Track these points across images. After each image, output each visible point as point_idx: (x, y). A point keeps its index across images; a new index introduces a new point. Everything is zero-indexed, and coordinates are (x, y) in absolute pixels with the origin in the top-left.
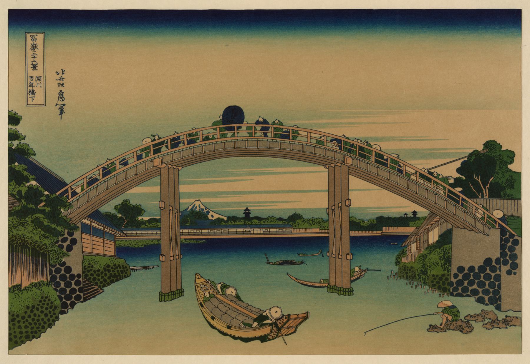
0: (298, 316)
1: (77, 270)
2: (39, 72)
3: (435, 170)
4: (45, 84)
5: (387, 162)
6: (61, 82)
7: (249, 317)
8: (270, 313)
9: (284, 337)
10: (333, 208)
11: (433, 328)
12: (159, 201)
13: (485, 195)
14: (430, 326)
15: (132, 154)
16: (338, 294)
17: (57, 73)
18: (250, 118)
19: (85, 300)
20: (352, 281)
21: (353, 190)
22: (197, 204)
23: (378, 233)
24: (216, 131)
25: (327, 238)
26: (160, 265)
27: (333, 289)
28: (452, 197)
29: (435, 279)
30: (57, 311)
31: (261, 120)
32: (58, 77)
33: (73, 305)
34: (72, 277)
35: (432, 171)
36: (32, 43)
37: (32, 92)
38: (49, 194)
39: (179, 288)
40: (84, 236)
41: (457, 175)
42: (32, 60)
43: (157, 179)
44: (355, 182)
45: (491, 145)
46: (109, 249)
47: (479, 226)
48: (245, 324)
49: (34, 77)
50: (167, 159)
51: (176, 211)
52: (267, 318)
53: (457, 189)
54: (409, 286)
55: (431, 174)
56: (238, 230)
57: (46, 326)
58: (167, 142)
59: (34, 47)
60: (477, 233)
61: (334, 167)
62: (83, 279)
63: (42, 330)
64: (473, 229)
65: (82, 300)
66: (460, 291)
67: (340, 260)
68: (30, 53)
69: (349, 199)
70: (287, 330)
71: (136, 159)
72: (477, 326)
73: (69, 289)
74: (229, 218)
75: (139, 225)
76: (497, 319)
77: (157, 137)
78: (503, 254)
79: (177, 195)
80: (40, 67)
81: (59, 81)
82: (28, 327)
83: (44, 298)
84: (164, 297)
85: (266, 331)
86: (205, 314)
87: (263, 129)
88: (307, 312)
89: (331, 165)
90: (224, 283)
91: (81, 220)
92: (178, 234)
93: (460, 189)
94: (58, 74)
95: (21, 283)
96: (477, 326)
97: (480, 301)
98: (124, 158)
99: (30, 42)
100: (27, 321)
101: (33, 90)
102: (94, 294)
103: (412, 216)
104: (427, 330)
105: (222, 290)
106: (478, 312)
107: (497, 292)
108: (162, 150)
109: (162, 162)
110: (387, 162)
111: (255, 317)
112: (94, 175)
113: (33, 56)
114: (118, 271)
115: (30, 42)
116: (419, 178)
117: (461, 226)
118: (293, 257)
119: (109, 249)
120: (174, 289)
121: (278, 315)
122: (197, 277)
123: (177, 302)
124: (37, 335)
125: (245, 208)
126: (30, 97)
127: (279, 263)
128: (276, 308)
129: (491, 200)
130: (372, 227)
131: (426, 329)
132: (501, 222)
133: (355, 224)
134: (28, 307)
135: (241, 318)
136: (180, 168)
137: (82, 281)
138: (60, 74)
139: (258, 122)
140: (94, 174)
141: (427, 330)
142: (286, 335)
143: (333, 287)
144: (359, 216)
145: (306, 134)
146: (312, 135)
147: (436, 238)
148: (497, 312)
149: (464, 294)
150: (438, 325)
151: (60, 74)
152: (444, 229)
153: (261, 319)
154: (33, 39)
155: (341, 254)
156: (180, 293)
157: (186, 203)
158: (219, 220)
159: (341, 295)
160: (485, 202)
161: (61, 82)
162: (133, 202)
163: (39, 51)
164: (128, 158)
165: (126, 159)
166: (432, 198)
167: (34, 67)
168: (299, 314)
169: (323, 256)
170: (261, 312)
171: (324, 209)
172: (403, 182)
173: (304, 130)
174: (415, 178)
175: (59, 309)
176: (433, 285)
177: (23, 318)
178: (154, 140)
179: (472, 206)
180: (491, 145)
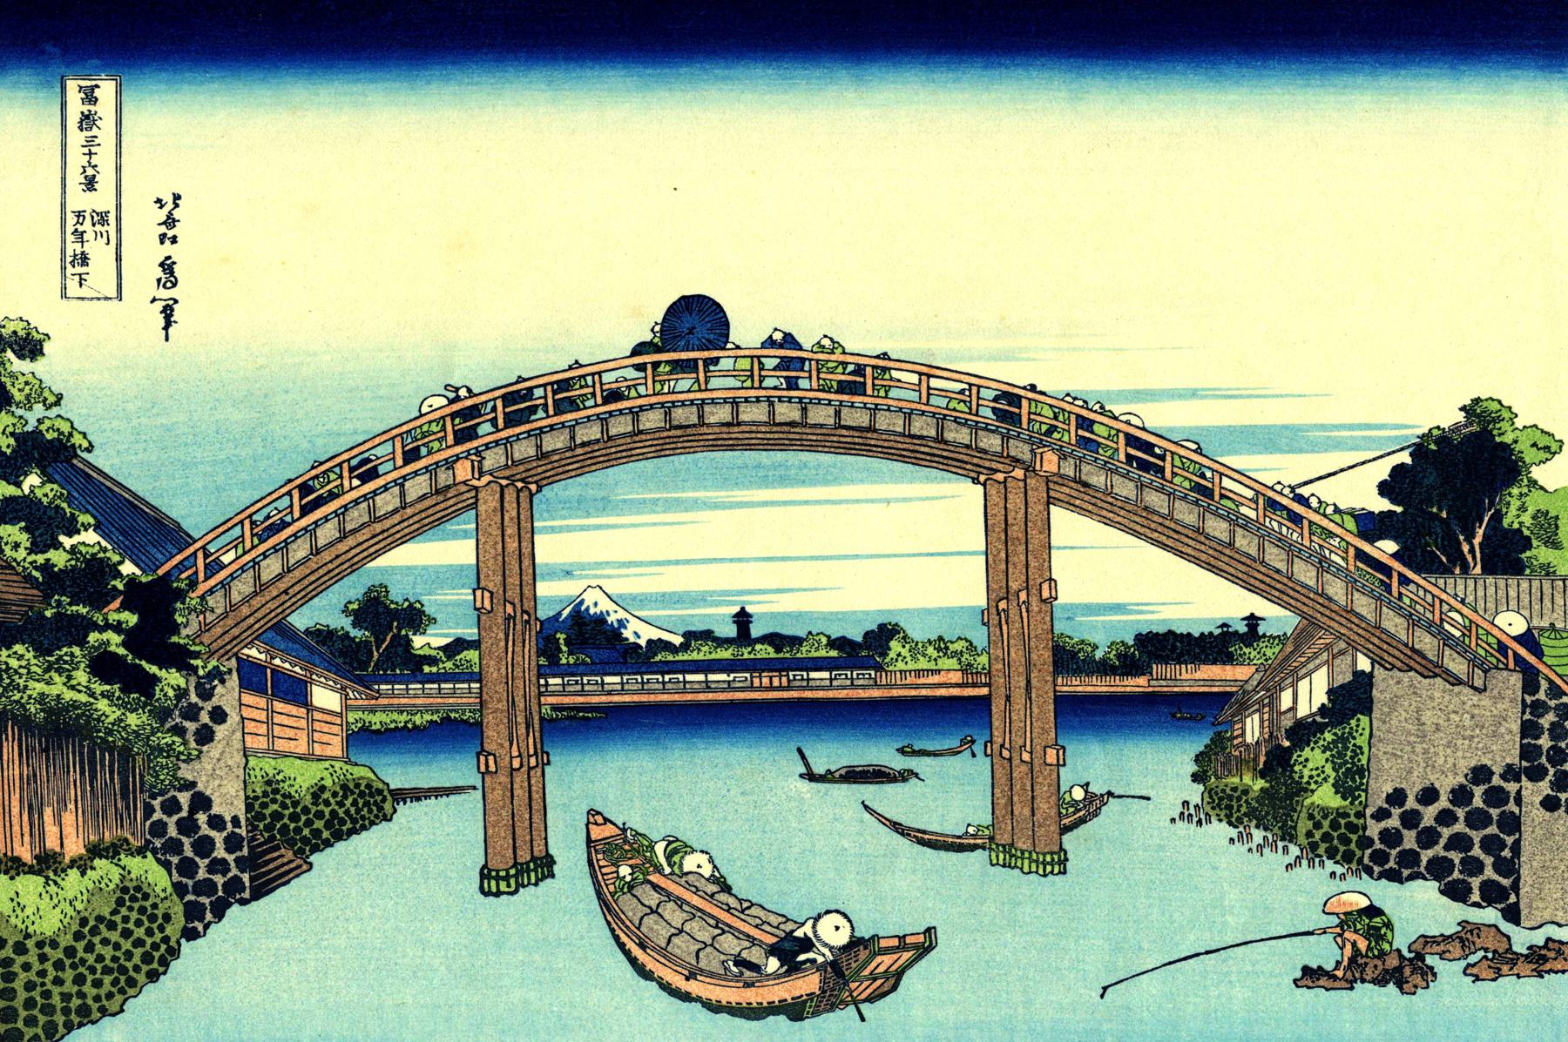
0: (902, 944)
1: (228, 800)
2: (102, 199)
4: (119, 230)
5: (1161, 463)
7: (753, 941)
8: (815, 932)
9: (863, 1007)
10: (1003, 605)
11: (1311, 976)
12: (474, 590)
13: (1472, 565)
14: (1306, 970)
15: (388, 448)
16: (1021, 869)
17: (159, 201)
18: (747, 330)
19: (258, 894)
20: (1066, 830)
21: (1059, 548)
22: (590, 598)
23: (1136, 684)
24: (643, 374)
25: (986, 701)
26: (479, 785)
29: (1318, 826)
30: (173, 930)
31: (778, 336)
32: (162, 215)
33: (219, 912)
34: (217, 822)
35: (1305, 491)
37: (84, 259)
38: (138, 572)
39: (539, 851)
40: (248, 698)
41: (1382, 505)
43: (467, 523)
44: (1067, 525)
45: (1472, 410)
46: (326, 738)
47: (1457, 665)
48: (740, 962)
50: (493, 459)
52: (806, 944)
53: (1382, 544)
54: (1239, 848)
55: (1302, 500)
56: (712, 677)
57: (141, 978)
58: (494, 409)
59: (87, 120)
60: (1425, 677)
62: (248, 832)
63: (131, 992)
64: (1437, 670)
65: (247, 895)
66: (1391, 864)
67: (1024, 768)
68: (76, 138)
69: (1051, 579)
70: (868, 983)
71: (400, 462)
72: (1449, 972)
73: (207, 861)
74: (689, 636)
75: (413, 666)
77: (463, 393)
78: (1528, 752)
79: (526, 567)
80: (106, 181)
81: (163, 229)
82: (94, 973)
83: (132, 893)
84: (493, 881)
85: (808, 984)
86: (618, 932)
87: (785, 363)
88: (928, 930)
89: (994, 477)
90: (677, 840)
91: (236, 650)
92: (534, 690)
93: (1390, 546)
94: (161, 207)
96: (1449, 972)
97: (1456, 892)
98: (366, 455)
99: (76, 106)
100: (83, 961)
101: (83, 253)
102: (282, 878)
103: (1242, 629)
104: (1295, 981)
105: (668, 858)
106: (1452, 929)
107: (1508, 867)
108: (482, 430)
109: (480, 469)
110: (1161, 463)
111: (771, 940)
112: (275, 512)
113: (86, 150)
115: (76, 106)
116: (1265, 516)
117: (1399, 664)
118: (882, 753)
119: (326, 738)
120: (524, 856)
121: (842, 938)
122: (592, 820)
124: (113, 1006)
125: (737, 609)
127: (841, 775)
128: (834, 915)
129: (1490, 580)
131: (1292, 978)
132: (1523, 652)
133: (1067, 658)
135: (730, 944)
136: (533, 487)
137: (244, 834)
139: (770, 343)
140: (275, 505)
141: (1295, 981)
142: (870, 999)
143: (1034, 869)
144: (1074, 630)
145: (914, 378)
146: (934, 383)
147: (1321, 698)
148: (1506, 927)
149: (1406, 873)
150: (1329, 966)
152: (1345, 677)
153: (791, 950)
155: (1007, 745)
156: (544, 866)
157: (552, 593)
158: (656, 645)
159: (1030, 872)
160: (1460, 587)
162: (398, 594)
163: (105, 131)
164: (378, 458)
165: (372, 461)
167: (90, 184)
168: (905, 936)
169: (974, 755)
170: (789, 927)
171: (973, 608)
172: (1217, 528)
174: (1252, 515)
175: (179, 920)
176: (1348, 858)
177: (70, 952)
178: (457, 399)
179: (1421, 593)
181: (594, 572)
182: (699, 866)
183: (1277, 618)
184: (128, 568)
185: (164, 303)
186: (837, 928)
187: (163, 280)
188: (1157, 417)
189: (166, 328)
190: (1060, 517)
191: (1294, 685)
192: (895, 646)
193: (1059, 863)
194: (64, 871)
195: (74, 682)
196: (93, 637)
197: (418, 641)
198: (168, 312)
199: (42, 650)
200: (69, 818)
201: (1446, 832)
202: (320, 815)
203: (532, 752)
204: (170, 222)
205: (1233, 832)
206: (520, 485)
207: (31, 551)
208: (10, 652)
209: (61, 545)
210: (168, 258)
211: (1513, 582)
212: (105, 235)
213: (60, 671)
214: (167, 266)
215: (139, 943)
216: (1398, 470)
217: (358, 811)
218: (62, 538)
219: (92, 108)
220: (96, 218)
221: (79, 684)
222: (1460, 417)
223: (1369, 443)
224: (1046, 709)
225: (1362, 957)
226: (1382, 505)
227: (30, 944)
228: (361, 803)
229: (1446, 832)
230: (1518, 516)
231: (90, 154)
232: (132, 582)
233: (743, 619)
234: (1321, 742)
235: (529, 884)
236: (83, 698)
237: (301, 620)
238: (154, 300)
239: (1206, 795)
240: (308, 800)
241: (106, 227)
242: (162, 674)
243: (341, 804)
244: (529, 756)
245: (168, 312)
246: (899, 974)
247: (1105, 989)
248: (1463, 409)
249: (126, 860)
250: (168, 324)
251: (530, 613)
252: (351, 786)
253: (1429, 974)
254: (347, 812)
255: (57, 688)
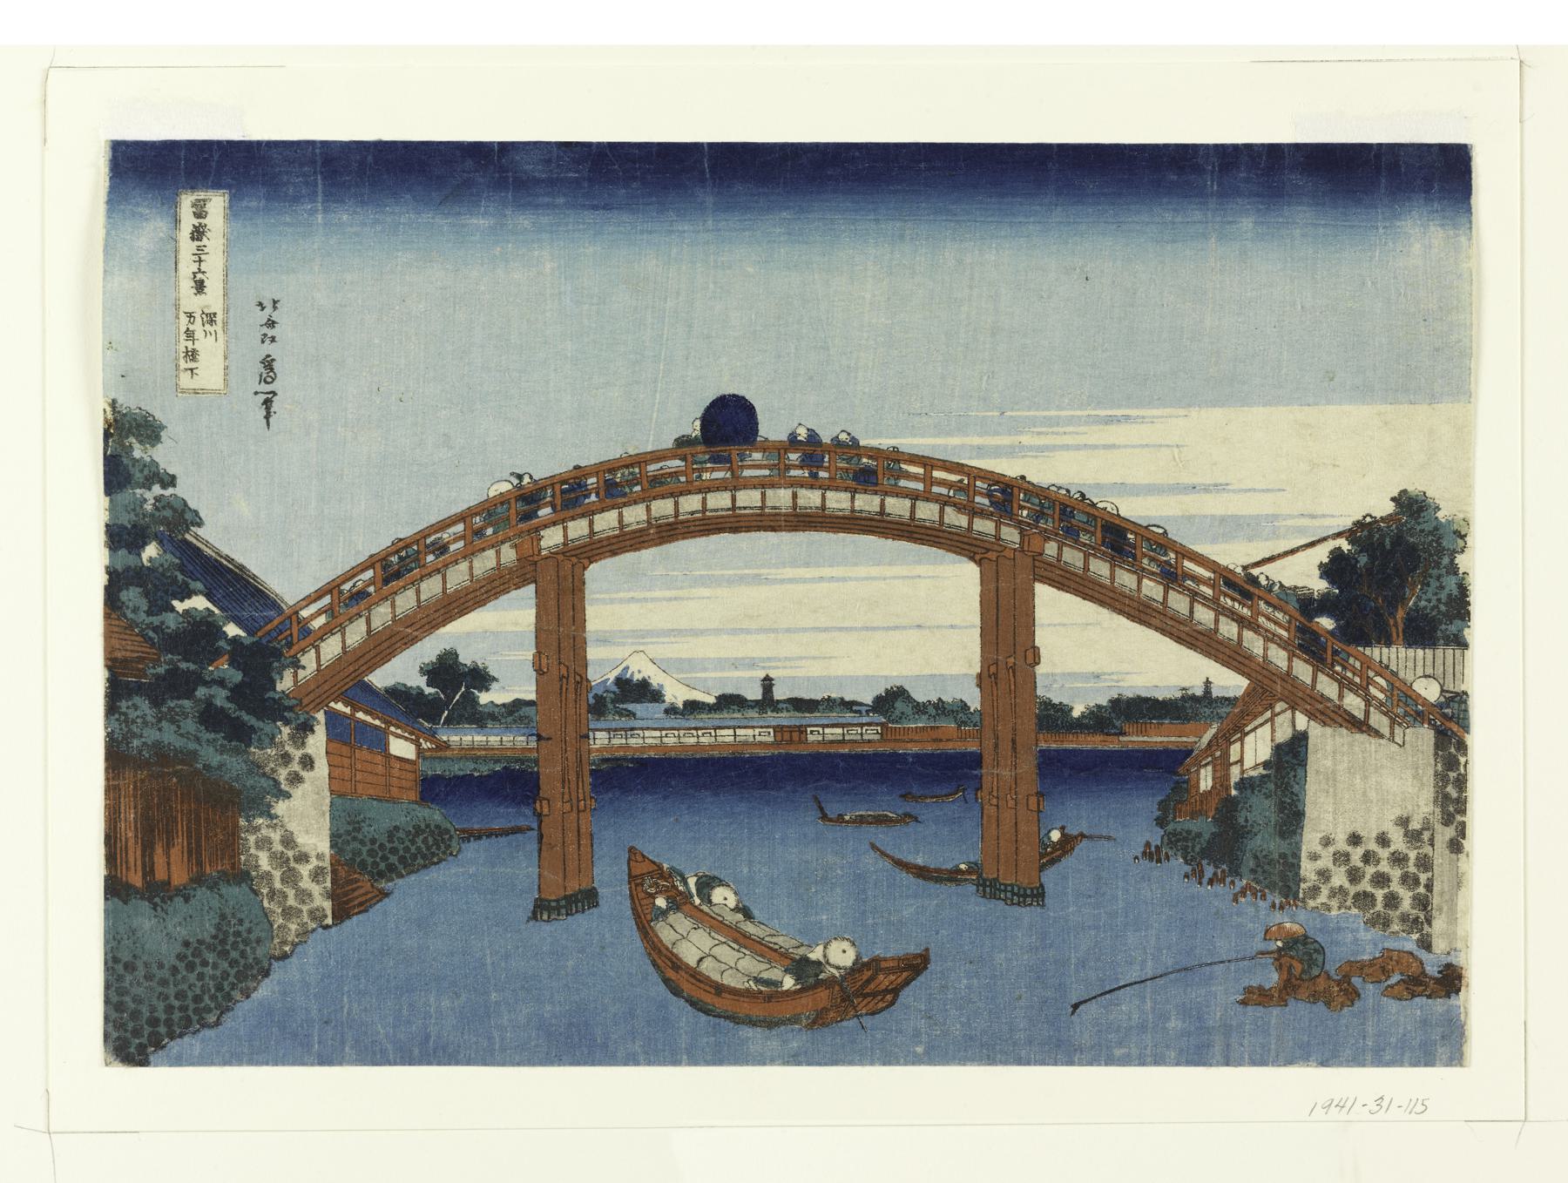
3: (1267, 569)
6: (270, 333)
8: (825, 956)
11: (1256, 997)
14: (1249, 990)
17: (260, 304)
18: (772, 428)
23: (1113, 744)
27: (990, 888)
28: (1310, 646)
32: (263, 317)
36: (196, 222)
37: (192, 355)
38: (243, 634)
42: (195, 267)
45: (1411, 506)
47: (1378, 720)
49: (198, 316)
51: (578, 678)
61: (997, 561)
72: (1370, 991)
75: (480, 718)
76: (1424, 973)
81: (265, 330)
84: (542, 909)
94: (263, 309)
95: (169, 878)
114: (425, 841)
115: (188, 221)
118: (889, 804)
123: (582, 922)
124: (212, 1018)
125: (763, 675)
126: (186, 369)
130: (1098, 720)
134: (186, 944)
138: (269, 310)
147: (1265, 753)
151: (269, 310)
152: (1284, 734)
154: (200, 214)
156: (588, 898)
161: (270, 333)
166: (1254, 644)
167: (200, 287)
173: (914, 459)
180: (1411, 506)
181: (631, 594)
182: (726, 899)
183: (1230, 683)
184: (232, 630)
185: (266, 396)
186: (844, 952)
187: (264, 375)
188: (1132, 509)
189: (267, 417)
190: (1043, 592)
191: (1241, 740)
192: (899, 705)
193: (1037, 895)
194: (171, 899)
195: (182, 731)
196: (201, 692)
197: (484, 698)
198: (267, 403)
199: (156, 703)
200: (175, 852)
201: (1370, 870)
202: (394, 851)
203: (581, 797)
204: (271, 324)
205: (1188, 869)
206: (574, 560)
207: (149, 613)
208: (130, 703)
209: (173, 609)
210: (268, 356)
211: (1429, 652)
212: (213, 333)
213: (173, 721)
214: (268, 364)
215: (233, 963)
216: (1337, 555)
217: (428, 848)
218: (175, 603)
219: (201, 220)
220: (205, 319)
221: (188, 733)
222: (1390, 508)
223: (1301, 531)
224: (1028, 765)
225: (1297, 979)
226: (1319, 586)
227: (139, 964)
228: (430, 839)
229: (1370, 870)
230: (1436, 594)
231: (200, 261)
232: (235, 640)
233: (768, 683)
234: (1264, 790)
235: (577, 912)
236: (192, 746)
237: (380, 678)
238: (256, 393)
239: (1166, 838)
240: (383, 839)
241: (214, 328)
242: (261, 724)
243: (413, 842)
244: (579, 801)
245: (267, 403)
246: (896, 992)
247: (1076, 1007)
248: (1393, 499)
249: (224, 890)
250: (267, 417)
251: (582, 681)
252: (423, 826)
253: (1352, 995)
254: (419, 848)
255: (169, 735)
